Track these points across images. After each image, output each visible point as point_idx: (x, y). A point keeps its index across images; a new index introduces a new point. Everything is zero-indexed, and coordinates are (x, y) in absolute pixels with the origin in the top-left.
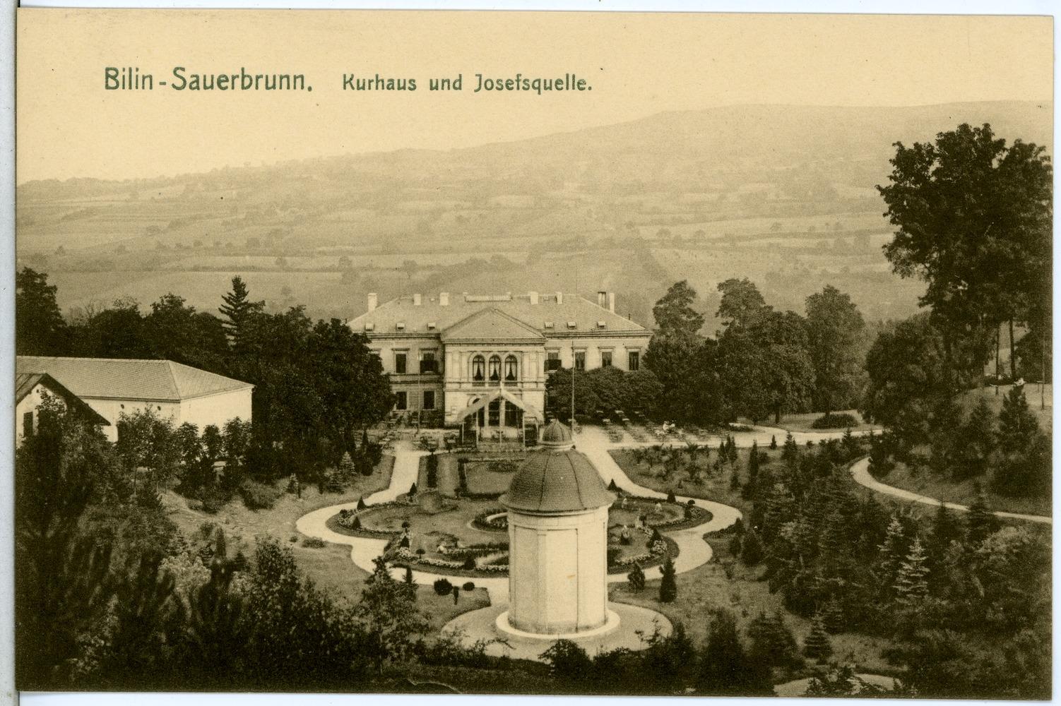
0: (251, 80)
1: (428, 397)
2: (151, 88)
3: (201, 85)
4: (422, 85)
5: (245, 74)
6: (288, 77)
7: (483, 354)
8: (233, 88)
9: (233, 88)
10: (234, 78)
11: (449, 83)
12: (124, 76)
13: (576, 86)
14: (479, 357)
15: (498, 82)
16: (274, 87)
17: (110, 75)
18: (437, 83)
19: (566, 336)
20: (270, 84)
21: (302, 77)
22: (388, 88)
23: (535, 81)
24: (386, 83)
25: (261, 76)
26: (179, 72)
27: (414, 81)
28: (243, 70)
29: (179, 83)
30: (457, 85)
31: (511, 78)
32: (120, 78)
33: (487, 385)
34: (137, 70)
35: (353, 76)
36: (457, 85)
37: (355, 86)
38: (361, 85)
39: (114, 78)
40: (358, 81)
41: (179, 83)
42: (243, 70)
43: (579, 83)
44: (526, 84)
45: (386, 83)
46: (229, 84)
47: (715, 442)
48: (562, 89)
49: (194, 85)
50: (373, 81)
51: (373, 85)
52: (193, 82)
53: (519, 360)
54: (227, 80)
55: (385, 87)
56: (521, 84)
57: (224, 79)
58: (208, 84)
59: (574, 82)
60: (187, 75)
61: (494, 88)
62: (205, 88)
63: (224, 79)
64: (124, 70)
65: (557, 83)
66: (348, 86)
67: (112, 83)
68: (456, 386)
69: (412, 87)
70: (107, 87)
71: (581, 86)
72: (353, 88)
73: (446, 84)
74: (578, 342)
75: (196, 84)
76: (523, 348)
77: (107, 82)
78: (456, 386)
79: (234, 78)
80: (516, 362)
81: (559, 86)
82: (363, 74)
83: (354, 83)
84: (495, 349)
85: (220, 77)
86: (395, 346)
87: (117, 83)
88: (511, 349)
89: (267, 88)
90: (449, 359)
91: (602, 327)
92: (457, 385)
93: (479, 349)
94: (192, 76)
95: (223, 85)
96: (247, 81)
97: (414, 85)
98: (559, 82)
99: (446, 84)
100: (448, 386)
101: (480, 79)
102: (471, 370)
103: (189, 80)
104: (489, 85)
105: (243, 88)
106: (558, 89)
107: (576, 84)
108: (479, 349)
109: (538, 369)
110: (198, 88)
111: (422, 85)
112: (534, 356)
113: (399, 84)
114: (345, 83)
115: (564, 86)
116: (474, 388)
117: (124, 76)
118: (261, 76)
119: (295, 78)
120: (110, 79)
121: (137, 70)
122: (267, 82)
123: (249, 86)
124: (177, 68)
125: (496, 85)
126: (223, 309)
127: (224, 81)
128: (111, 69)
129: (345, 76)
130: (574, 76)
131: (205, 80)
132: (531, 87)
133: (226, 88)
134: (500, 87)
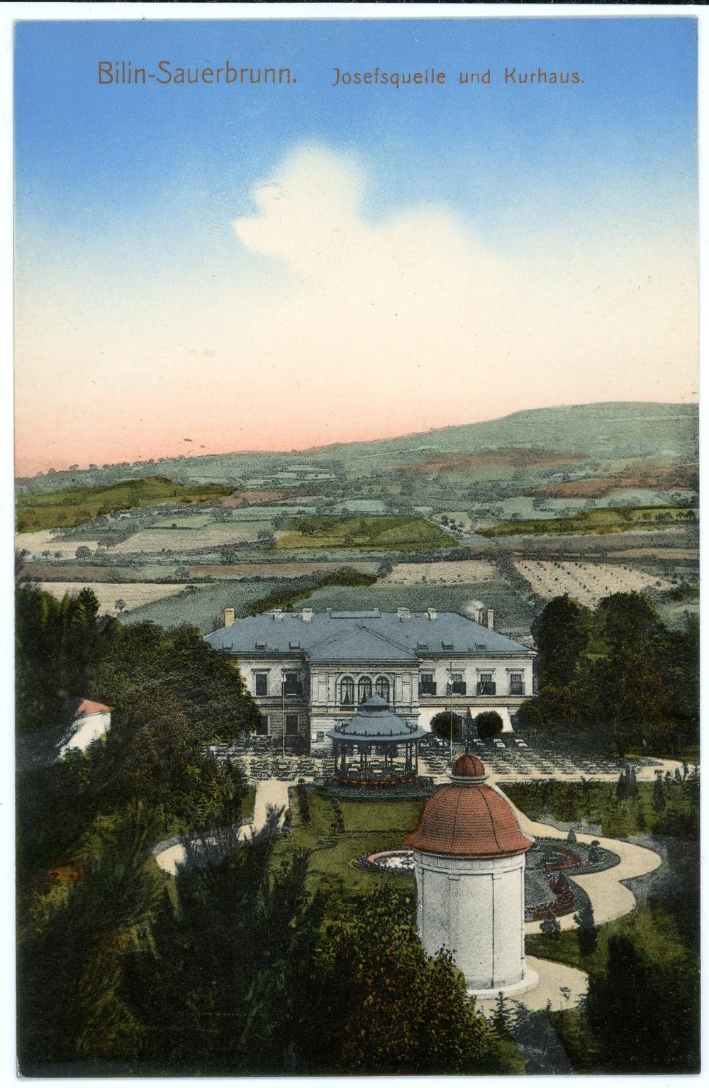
0: (483, 81)
1: (291, 723)
3: (186, 80)
5: (542, 72)
7: (369, 676)
13: (200, 79)
14: (346, 678)
20: (255, 78)
24: (548, 77)
29: (165, 77)
31: (369, 72)
32: (113, 72)
36: (486, 79)
37: (517, 80)
38: (523, 79)
41: (165, 77)
43: (439, 77)
44: (384, 78)
46: (214, 78)
49: (179, 79)
51: (535, 78)
56: (380, 78)
57: (209, 72)
58: (407, 79)
59: (433, 75)
61: (352, 81)
63: (209, 72)
64: (117, 64)
67: (105, 77)
68: (322, 711)
74: (456, 664)
76: (393, 670)
78: (322, 711)
83: (516, 76)
84: (365, 671)
86: (255, 667)
88: (383, 671)
90: (314, 680)
93: (348, 671)
97: (577, 78)
100: (314, 711)
101: (338, 73)
104: (347, 78)
107: (435, 78)
109: (411, 692)
110: (183, 81)
112: (406, 678)
114: (507, 77)
115: (423, 79)
118: (247, 70)
119: (281, 71)
122: (252, 76)
124: (161, 63)
125: (353, 78)
131: (562, 77)
132: (389, 81)
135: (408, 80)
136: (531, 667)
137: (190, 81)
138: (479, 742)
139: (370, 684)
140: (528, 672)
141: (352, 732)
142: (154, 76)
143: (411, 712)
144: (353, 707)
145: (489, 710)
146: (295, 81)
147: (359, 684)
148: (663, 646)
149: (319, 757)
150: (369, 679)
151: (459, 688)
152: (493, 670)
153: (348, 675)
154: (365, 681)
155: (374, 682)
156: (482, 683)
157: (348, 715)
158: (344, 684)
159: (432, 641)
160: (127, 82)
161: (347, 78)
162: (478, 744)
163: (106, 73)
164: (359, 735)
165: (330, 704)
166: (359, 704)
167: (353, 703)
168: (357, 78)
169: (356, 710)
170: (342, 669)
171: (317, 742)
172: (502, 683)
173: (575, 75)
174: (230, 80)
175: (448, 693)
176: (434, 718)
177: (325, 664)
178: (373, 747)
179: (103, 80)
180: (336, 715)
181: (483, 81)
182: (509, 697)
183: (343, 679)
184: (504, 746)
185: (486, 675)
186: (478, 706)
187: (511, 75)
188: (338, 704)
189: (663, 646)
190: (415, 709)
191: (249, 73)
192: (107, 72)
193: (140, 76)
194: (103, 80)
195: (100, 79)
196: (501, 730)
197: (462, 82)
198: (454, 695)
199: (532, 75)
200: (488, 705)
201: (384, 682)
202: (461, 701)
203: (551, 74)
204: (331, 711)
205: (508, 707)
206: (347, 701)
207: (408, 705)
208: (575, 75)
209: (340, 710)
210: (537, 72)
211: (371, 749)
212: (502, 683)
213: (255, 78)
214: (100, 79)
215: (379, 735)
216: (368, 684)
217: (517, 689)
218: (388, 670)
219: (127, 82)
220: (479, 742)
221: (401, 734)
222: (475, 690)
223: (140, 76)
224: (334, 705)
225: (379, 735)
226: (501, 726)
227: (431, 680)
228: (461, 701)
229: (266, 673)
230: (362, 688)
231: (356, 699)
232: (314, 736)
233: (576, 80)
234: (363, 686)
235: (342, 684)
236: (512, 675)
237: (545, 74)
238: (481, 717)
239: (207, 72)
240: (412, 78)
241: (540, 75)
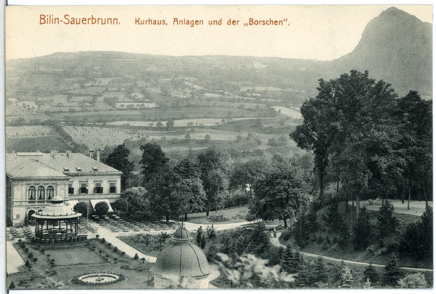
2: (55, 23)
4: (206, 22)
6: (111, 19)
7: (34, 185)
8: (88, 24)
9: (88, 24)
10: (89, 19)
11: (77, 23)
12: (47, 19)
14: (32, 187)
15: (163, 21)
18: (214, 23)
19: (77, 175)
20: (103, 22)
21: (202, 21)
23: (228, 22)
24: (153, 22)
25: (100, 19)
26: (66, 17)
27: (164, 21)
28: (92, 16)
29: (67, 21)
30: (220, 23)
32: (46, 19)
33: (36, 203)
34: (53, 16)
35: (139, 19)
36: (220, 23)
37: (140, 23)
38: (142, 23)
41: (67, 21)
42: (92, 16)
45: (153, 22)
46: (87, 22)
47: (170, 231)
48: (235, 24)
49: (73, 22)
50: (147, 21)
51: (148, 22)
52: (72, 21)
53: (55, 189)
54: (86, 20)
55: (152, 23)
57: (84, 19)
58: (78, 22)
60: (69, 18)
63: (84, 19)
64: (47, 16)
65: (196, 22)
66: (137, 23)
67: (43, 21)
69: (164, 23)
71: (84, 22)
73: (215, 22)
74: (83, 179)
75: (73, 21)
79: (89, 19)
80: (53, 190)
81: (234, 23)
82: (143, 18)
83: (140, 21)
85: (83, 19)
87: (45, 21)
88: (50, 183)
89: (102, 24)
92: (20, 203)
94: (72, 19)
96: (93, 20)
98: (276, 21)
99: (215, 22)
100: (15, 204)
102: (28, 194)
103: (70, 20)
104: (256, 23)
106: (233, 24)
110: (156, 24)
112: (63, 187)
114: (136, 21)
116: (29, 204)
117: (47, 19)
118: (100, 19)
119: (114, 19)
120: (41, 19)
121: (53, 16)
126: (26, 132)
127: (84, 20)
128: (42, 15)
129: (136, 19)
133: (235, 24)
134: (264, 24)
138: (96, 216)
139: (35, 190)
141: (47, 215)
142: (62, 21)
143: (22, 204)
144: (44, 201)
146: (119, 23)
147: (47, 190)
148: (182, 169)
152: (101, 181)
155: (37, 189)
156: (96, 187)
158: (48, 190)
161: (256, 23)
162: (96, 218)
163: (43, 20)
164: (50, 216)
165: (23, 200)
166: (47, 199)
167: (44, 199)
169: (46, 202)
170: (29, 182)
171: (16, 219)
172: (106, 186)
174: (93, 23)
176: (75, 206)
179: (42, 22)
180: (26, 206)
183: (30, 188)
184: (109, 218)
185: (112, 184)
186: (94, 199)
187: (138, 21)
188: (27, 200)
189: (182, 169)
190: (67, 201)
192: (42, 19)
193: (57, 20)
194: (42, 22)
195: (40, 22)
197: (209, 24)
198: (82, 194)
199: (146, 21)
202: (86, 197)
203: (72, 19)
205: (109, 199)
206: (31, 198)
207: (21, 200)
209: (38, 203)
213: (103, 22)
214: (40, 22)
215: (61, 215)
216: (52, 190)
217: (113, 190)
223: (57, 20)
224: (25, 201)
225: (61, 215)
226: (108, 209)
228: (86, 197)
229: (100, 183)
231: (46, 197)
232: (15, 217)
233: (164, 23)
234: (40, 191)
235: (29, 190)
236: (111, 184)
237: (272, 21)
238: (97, 205)
239: (84, 19)
241: (149, 21)
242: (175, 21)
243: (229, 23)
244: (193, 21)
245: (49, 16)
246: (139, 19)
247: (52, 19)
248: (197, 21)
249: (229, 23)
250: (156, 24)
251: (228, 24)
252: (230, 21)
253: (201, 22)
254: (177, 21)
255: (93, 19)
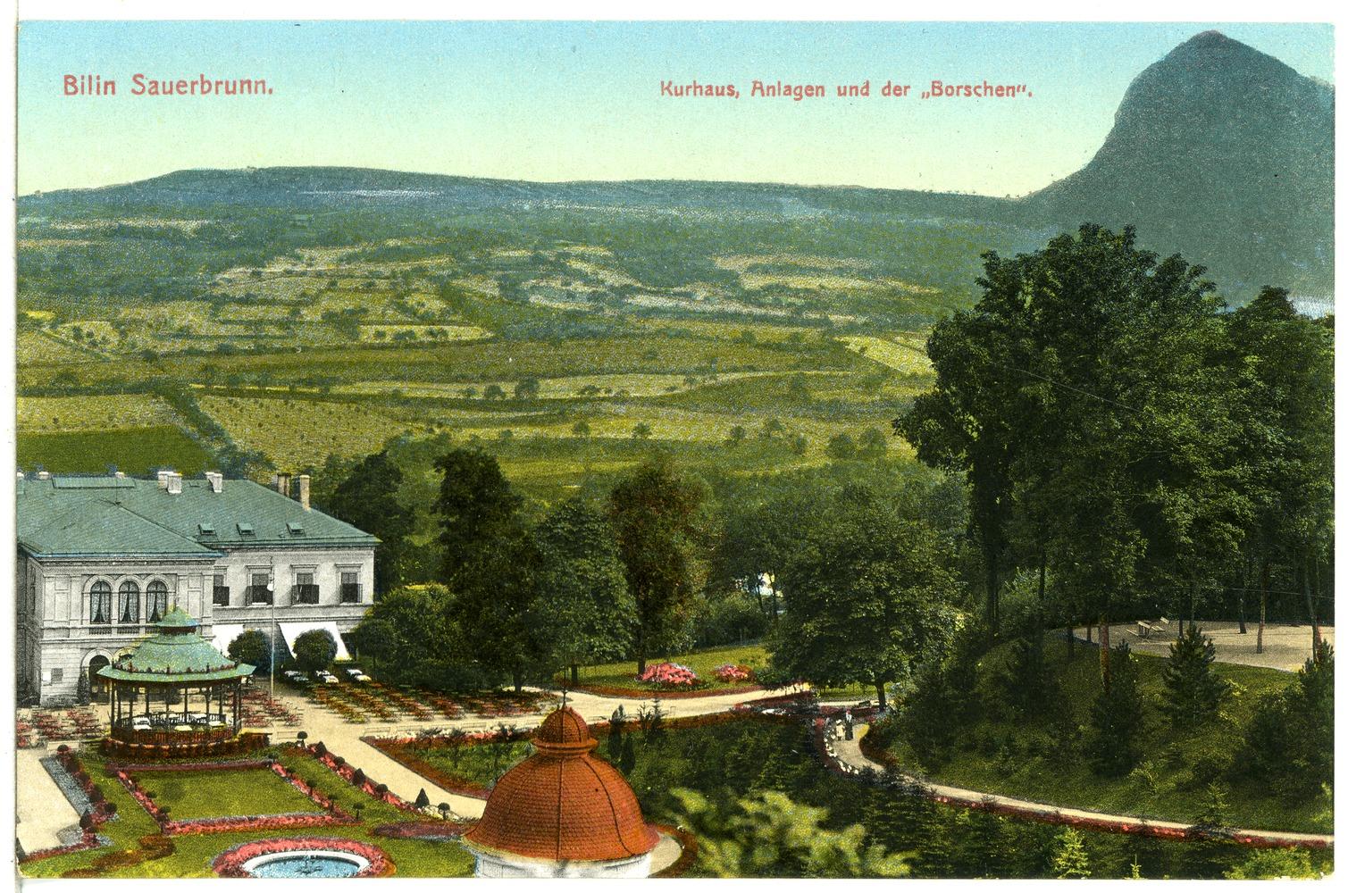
4: (831, 91)
5: (205, 78)
7: (135, 578)
16: (234, 92)
17: (69, 81)
22: (785, 94)
24: (705, 89)
25: (221, 83)
26: (139, 79)
32: (78, 84)
37: (673, 92)
39: (73, 84)
40: (676, 88)
41: (139, 88)
45: (705, 89)
46: (189, 89)
50: (197, 82)
54: (186, 85)
60: (145, 82)
62: (718, 94)
64: (83, 77)
67: (71, 89)
70: (67, 93)
72: (671, 94)
73: (854, 91)
77: (66, 88)
79: (193, 83)
84: (131, 572)
87: (76, 87)
88: (158, 573)
91: (297, 532)
93: (101, 573)
95: (182, 89)
98: (182, 84)
99: (854, 91)
100: (48, 636)
103: (148, 87)
105: (203, 92)
108: (101, 573)
111: (831, 91)
113: (249, 87)
118: (221, 83)
121: (98, 78)
123: (796, 88)
130: (98, 78)
131: (90, 89)
135: (220, 86)
136: (372, 561)
137: (164, 93)
140: (366, 570)
145: (317, 626)
148: (563, 528)
149: (57, 708)
150: (107, 584)
151: (259, 593)
153: (102, 578)
154: (130, 589)
157: (130, 640)
159: (223, 525)
160: (94, 92)
167: (138, 622)
168: (139, 83)
172: (328, 584)
173: (730, 87)
175: (246, 602)
177: (61, 561)
178: (142, 690)
180: (83, 642)
181: (210, 84)
182: (338, 606)
187: (667, 88)
191: (224, 86)
192: (71, 84)
196: (334, 656)
200: (316, 620)
201: (159, 589)
203: (151, 83)
204: (74, 635)
206: (99, 619)
208: (730, 87)
210: (199, 79)
211: (137, 692)
212: (328, 584)
213: (231, 88)
215: (189, 672)
217: (349, 592)
218: (169, 568)
219: (94, 92)
220: (297, 675)
221: (189, 672)
222: (242, 599)
227: (222, 583)
230: (96, 598)
231: (143, 615)
237: (701, 87)
240: (174, 87)
241: (696, 87)
242: (755, 88)
243: (887, 91)
244: (801, 87)
245: (86, 79)
246: (670, 83)
247: (98, 85)
248: (810, 87)
249: (887, 91)
250: (157, 93)
251: (885, 95)
252: (889, 86)
253: (820, 91)
254: (761, 88)
255: (203, 83)
